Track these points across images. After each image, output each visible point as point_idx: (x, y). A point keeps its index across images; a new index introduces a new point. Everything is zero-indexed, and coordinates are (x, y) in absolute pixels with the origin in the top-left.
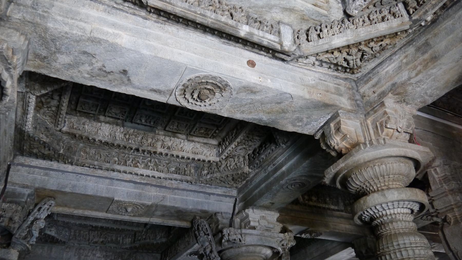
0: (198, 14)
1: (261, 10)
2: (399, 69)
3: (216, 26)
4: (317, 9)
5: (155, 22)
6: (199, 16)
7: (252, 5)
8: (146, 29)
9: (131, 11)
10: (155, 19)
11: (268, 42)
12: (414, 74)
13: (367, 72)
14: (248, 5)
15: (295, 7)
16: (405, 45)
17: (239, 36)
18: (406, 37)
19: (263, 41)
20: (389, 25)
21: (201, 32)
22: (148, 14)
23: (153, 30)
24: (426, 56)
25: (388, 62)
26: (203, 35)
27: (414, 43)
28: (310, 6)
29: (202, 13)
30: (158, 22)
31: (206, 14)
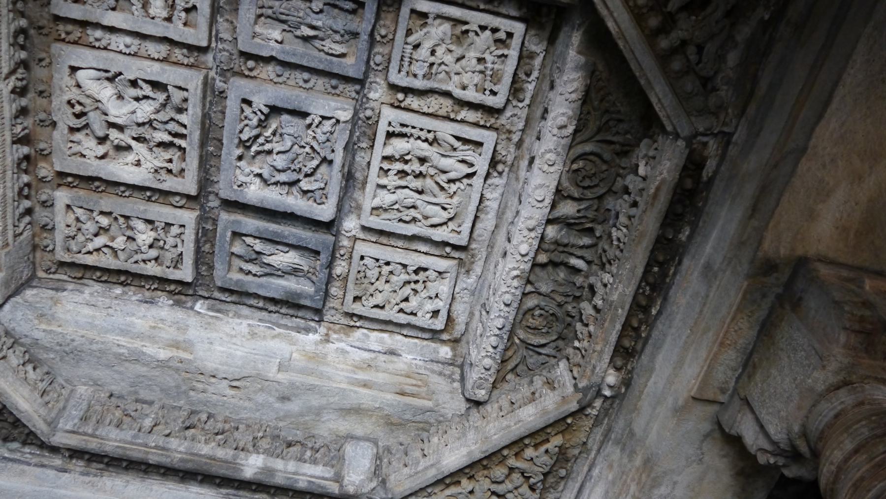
0: (151, 448)
1: (302, 420)
3: (189, 466)
5: (83, 474)
7: (282, 414)
8: (56, 490)
9: (35, 460)
10: (82, 469)
11: (309, 482)
14: (273, 415)
17: (242, 478)
19: (296, 481)
20: (539, 407)
21: (175, 481)
22: (68, 461)
23: (73, 491)
26: (181, 486)
28: (390, 397)
29: (161, 444)
30: (87, 474)
31: (169, 446)
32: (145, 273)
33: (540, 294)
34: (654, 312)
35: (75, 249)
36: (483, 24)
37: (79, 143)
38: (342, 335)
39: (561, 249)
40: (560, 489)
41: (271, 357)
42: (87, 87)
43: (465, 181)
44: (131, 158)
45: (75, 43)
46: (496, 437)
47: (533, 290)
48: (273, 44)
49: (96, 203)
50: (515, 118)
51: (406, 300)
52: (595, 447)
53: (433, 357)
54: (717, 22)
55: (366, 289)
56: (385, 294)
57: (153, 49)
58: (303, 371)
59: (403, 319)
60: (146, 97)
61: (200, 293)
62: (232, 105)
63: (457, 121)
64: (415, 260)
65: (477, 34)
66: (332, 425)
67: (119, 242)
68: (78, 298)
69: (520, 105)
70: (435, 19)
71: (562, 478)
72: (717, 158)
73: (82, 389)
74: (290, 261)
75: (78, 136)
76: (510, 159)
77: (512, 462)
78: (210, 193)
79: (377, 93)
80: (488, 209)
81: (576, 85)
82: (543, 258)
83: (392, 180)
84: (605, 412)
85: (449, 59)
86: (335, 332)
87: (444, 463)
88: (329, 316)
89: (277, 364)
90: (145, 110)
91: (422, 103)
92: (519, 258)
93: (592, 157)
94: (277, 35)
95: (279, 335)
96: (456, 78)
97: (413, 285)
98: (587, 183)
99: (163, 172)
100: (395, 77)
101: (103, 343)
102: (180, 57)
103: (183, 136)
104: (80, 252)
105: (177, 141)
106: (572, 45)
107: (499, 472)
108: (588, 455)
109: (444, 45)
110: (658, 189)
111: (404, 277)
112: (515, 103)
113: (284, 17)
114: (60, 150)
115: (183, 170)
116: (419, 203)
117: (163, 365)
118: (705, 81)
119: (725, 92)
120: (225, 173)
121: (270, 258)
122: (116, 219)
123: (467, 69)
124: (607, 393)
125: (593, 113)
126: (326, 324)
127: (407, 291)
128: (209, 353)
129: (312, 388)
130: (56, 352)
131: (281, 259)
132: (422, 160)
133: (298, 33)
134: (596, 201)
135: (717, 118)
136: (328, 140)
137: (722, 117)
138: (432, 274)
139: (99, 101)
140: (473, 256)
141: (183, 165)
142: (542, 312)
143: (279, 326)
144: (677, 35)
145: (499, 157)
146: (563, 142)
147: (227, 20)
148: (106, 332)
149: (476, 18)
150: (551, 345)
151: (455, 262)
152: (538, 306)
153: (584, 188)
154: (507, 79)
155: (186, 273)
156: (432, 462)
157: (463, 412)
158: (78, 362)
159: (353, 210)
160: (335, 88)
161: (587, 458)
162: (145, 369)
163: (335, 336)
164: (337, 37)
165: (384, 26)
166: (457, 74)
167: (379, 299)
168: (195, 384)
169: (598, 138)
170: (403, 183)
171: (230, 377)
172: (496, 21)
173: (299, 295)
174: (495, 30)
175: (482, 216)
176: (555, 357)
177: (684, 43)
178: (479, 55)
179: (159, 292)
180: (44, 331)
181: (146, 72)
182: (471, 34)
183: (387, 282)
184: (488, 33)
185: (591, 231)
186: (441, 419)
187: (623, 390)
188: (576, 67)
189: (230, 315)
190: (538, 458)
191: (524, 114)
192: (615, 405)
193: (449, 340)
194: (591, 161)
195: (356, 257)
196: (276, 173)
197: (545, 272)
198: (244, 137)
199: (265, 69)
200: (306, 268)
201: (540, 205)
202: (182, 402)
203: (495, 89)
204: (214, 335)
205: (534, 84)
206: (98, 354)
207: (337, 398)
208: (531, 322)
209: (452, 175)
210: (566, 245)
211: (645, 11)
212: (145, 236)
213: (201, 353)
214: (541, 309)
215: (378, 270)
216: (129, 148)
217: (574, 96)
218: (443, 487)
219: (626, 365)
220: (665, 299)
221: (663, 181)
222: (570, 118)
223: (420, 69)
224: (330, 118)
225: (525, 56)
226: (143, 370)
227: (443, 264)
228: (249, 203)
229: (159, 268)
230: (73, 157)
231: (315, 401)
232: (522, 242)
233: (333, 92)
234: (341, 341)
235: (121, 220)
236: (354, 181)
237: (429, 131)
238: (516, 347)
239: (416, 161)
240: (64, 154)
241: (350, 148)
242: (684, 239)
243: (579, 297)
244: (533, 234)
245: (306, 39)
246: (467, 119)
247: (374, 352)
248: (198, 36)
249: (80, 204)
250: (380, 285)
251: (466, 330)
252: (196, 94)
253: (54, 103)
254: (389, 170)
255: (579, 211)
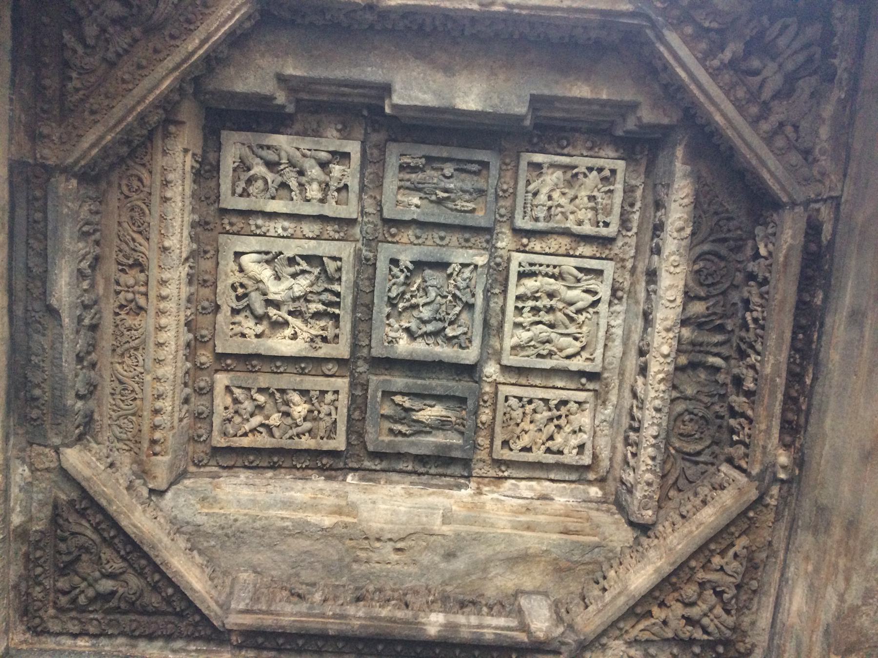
0: (329, 617)
1: (468, 580)
2: (814, 593)
4: (575, 538)
6: (332, 621)
7: (447, 575)
12: (842, 585)
13: (767, 637)
14: (438, 579)
15: (527, 549)
16: (789, 537)
18: (776, 521)
19: (482, 634)
20: (718, 506)
24: (837, 532)
25: (785, 590)
27: (800, 523)
29: (338, 611)
32: (300, 448)
33: (686, 398)
34: (808, 381)
35: (231, 432)
36: (590, 165)
37: (239, 323)
38: (493, 487)
39: (698, 348)
40: (754, 609)
41: (434, 509)
42: (250, 269)
43: (591, 310)
44: (288, 332)
45: (238, 233)
46: (680, 547)
47: (678, 395)
48: (413, 208)
49: (255, 380)
50: (626, 247)
51: (551, 438)
52: (783, 545)
53: (584, 496)
54: (805, 102)
55: (513, 432)
56: (531, 433)
57: (308, 229)
58: (465, 521)
59: (551, 459)
60: (303, 272)
61: (350, 465)
62: (382, 265)
63: (576, 256)
64: (554, 396)
65: (585, 176)
66: (503, 581)
67: (275, 419)
68: (234, 480)
69: (629, 234)
70: (548, 168)
71: (755, 592)
72: (832, 222)
73: (243, 576)
74: (438, 414)
75: (239, 318)
76: (626, 285)
77: (701, 575)
78: (359, 358)
79: (505, 241)
80: (614, 336)
81: (686, 191)
82: (683, 360)
83: (527, 318)
84: (783, 500)
85: (563, 201)
86: (485, 485)
87: (632, 587)
88: (477, 470)
89: (441, 514)
90: (302, 285)
91: (544, 245)
92: (662, 360)
93: (707, 257)
94: (416, 201)
95: (433, 493)
96: (571, 217)
97: (556, 422)
98: (710, 281)
99: (318, 340)
100: (521, 223)
101: (266, 518)
102: (332, 233)
103: (337, 305)
104: (235, 436)
105: (331, 310)
106: (677, 158)
107: (690, 591)
108: (776, 558)
109: (558, 190)
110: (786, 257)
111: (547, 414)
112: (624, 233)
113: (421, 186)
114: (223, 332)
115: (337, 336)
116: (553, 336)
117: (326, 533)
118: (807, 153)
119: (825, 162)
120: (377, 331)
121: (419, 413)
122: (273, 394)
123: (581, 206)
124: (782, 476)
125: (703, 216)
126: (475, 479)
127: (551, 428)
128: (373, 513)
129: (477, 538)
130: (218, 537)
131: (429, 413)
132: (551, 295)
133: (434, 198)
134: (721, 297)
135: (824, 184)
136: (468, 287)
137: (827, 183)
138: (573, 406)
139: (261, 281)
140: (607, 385)
141: (337, 331)
142: (692, 416)
143: (431, 486)
144: (774, 119)
145: (617, 285)
146: (684, 243)
147: (371, 196)
148: (268, 508)
149: (582, 163)
150: (707, 451)
151: (591, 393)
152: (687, 410)
153: (709, 286)
154: (617, 210)
155: (339, 443)
156: (618, 590)
157: (631, 544)
158: (239, 547)
159: (490, 356)
160: (467, 240)
161: (775, 563)
162: (308, 542)
163: (487, 489)
164: (467, 197)
165: (505, 182)
166: (572, 213)
167: (525, 440)
168: (359, 553)
169: (711, 238)
170: (537, 319)
171: (394, 536)
172: (600, 162)
173: (450, 447)
174: (600, 170)
175: (610, 344)
176: (713, 464)
177: (781, 125)
178: (589, 193)
179: (310, 472)
180: (207, 514)
181: (304, 248)
182: (581, 176)
183: (531, 422)
184: (595, 173)
185: (721, 329)
186: (611, 555)
187: (797, 472)
188: (685, 175)
189: (382, 482)
190: (727, 566)
191: (633, 241)
192: (793, 490)
193: (596, 480)
194: (709, 260)
195: (501, 398)
196: (422, 326)
197: (686, 376)
198: (393, 294)
199: (405, 235)
200: (453, 419)
201: (673, 305)
202: (344, 579)
203: (608, 220)
204: (374, 497)
205: (638, 214)
206: (260, 532)
207: (503, 546)
208: (683, 429)
209: (580, 305)
210: (701, 344)
211: (744, 102)
212: (300, 409)
213: (365, 514)
214: (692, 413)
215: (521, 411)
216: (286, 324)
217: (686, 201)
218: (632, 621)
219: (793, 442)
220: (817, 364)
221: (791, 248)
222: (686, 221)
223: (541, 213)
224: (468, 265)
225: (629, 190)
226: (305, 544)
227: (581, 396)
228: (400, 358)
229: (313, 440)
230: (234, 338)
231: (482, 552)
232: (662, 343)
233: (466, 245)
234: (493, 492)
235: (278, 395)
236: (489, 329)
237: (555, 267)
238: (672, 459)
239: (544, 296)
240: (227, 335)
241: (488, 293)
242: (819, 303)
243: (724, 395)
244: (671, 335)
245: (440, 202)
246: (584, 254)
247: (527, 498)
248: (350, 211)
249: (239, 384)
250: (525, 425)
251: (611, 466)
252: (349, 261)
253: (219, 288)
254: (523, 307)
255: (708, 308)
